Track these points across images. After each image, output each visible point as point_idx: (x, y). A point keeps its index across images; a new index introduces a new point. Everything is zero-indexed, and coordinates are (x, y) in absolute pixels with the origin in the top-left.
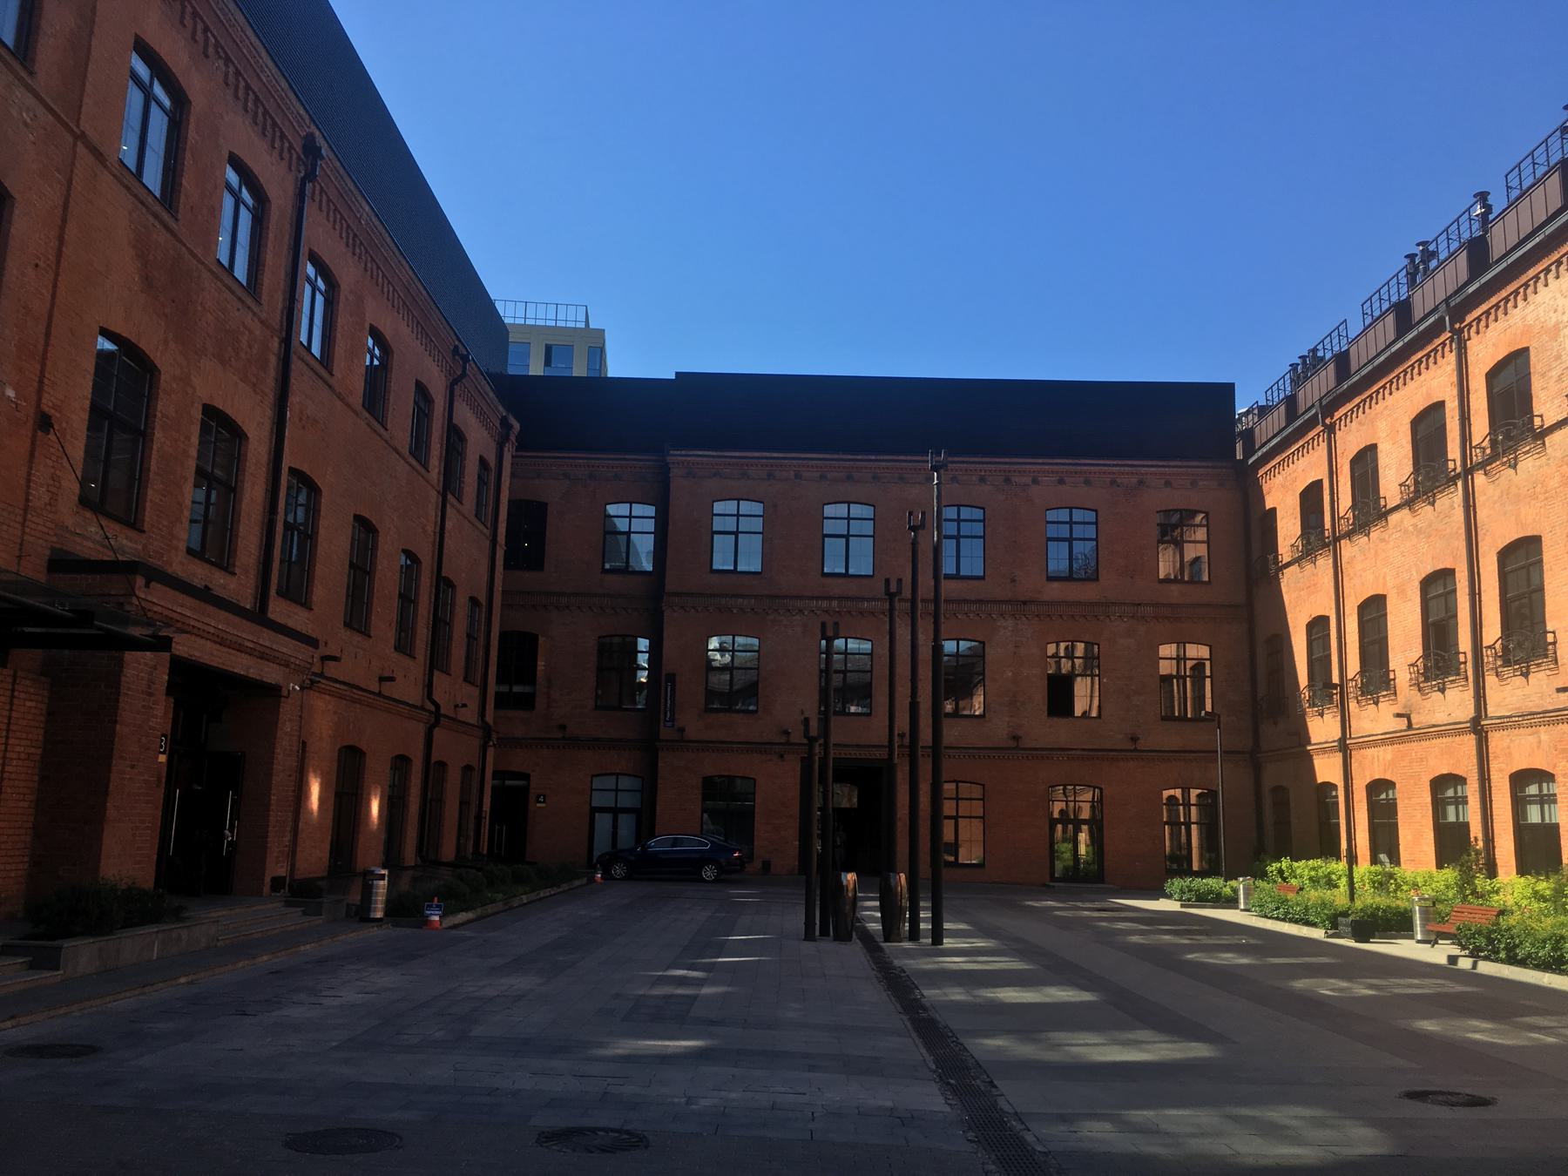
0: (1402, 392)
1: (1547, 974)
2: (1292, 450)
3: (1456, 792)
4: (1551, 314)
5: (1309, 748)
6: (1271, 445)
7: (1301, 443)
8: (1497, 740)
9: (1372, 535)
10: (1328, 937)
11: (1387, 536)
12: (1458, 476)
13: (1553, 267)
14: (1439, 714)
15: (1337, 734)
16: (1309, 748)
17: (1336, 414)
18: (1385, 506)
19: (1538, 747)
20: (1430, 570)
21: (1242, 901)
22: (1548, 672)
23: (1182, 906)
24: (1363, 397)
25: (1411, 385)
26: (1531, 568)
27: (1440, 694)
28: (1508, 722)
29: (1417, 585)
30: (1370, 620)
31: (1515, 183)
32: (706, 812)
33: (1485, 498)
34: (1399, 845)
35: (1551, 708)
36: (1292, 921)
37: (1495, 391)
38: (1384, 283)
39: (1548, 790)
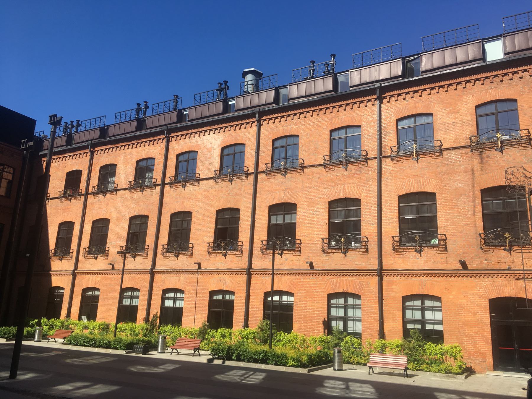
0: (134, 150)
1: (263, 365)
2: (222, 126)
3: (92, 293)
4: (209, 144)
5: (51, 272)
6: (136, 134)
7: (116, 145)
8: (157, 277)
9: (106, 196)
10: (126, 353)
11: (115, 198)
12: (83, 195)
13: (108, 149)
14: (130, 266)
15: (72, 268)
16: (51, 272)
17: (96, 148)
18: (49, 197)
19: (178, 281)
20: (136, 214)
21: (160, 348)
22: (187, 257)
23: (7, 341)
24: (242, 122)
25: (139, 149)
26: (184, 221)
27: (133, 258)
28: (164, 272)
29: (128, 218)
30: (96, 227)
31: (198, 99)
32: (528, 368)
33: (168, 194)
34: (97, 313)
35: (187, 269)
36: (98, 347)
37: (138, 167)
38: (199, 93)
39: (94, 293)
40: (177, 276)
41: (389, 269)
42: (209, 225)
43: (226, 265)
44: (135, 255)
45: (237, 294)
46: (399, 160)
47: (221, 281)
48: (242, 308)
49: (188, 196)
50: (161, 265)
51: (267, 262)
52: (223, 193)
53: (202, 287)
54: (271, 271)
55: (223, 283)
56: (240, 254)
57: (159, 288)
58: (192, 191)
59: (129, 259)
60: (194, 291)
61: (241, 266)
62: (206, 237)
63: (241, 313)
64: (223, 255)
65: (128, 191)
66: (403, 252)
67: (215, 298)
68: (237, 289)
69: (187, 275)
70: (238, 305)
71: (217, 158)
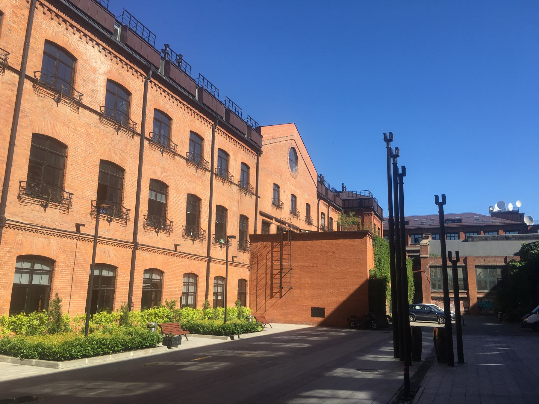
22: (61, 211)
40: (45, 238)
41: (201, 255)
42: (91, 176)
43: (110, 234)
44: (111, 219)
45: (121, 269)
46: (41, 92)
47: (104, 252)
48: (124, 287)
49: (63, 119)
50: (15, 214)
51: (147, 238)
52: (109, 142)
53: (82, 258)
54: (94, 238)
55: (107, 256)
56: (124, 223)
57: (11, 252)
58: (68, 114)
59: (103, 223)
60: (71, 262)
61: (125, 238)
62: (88, 190)
63: (124, 291)
64: (107, 220)
65: (98, 117)
66: (28, 203)
67: (48, 268)
68: (121, 264)
69: (61, 239)
70: (121, 283)
71: (102, 89)
